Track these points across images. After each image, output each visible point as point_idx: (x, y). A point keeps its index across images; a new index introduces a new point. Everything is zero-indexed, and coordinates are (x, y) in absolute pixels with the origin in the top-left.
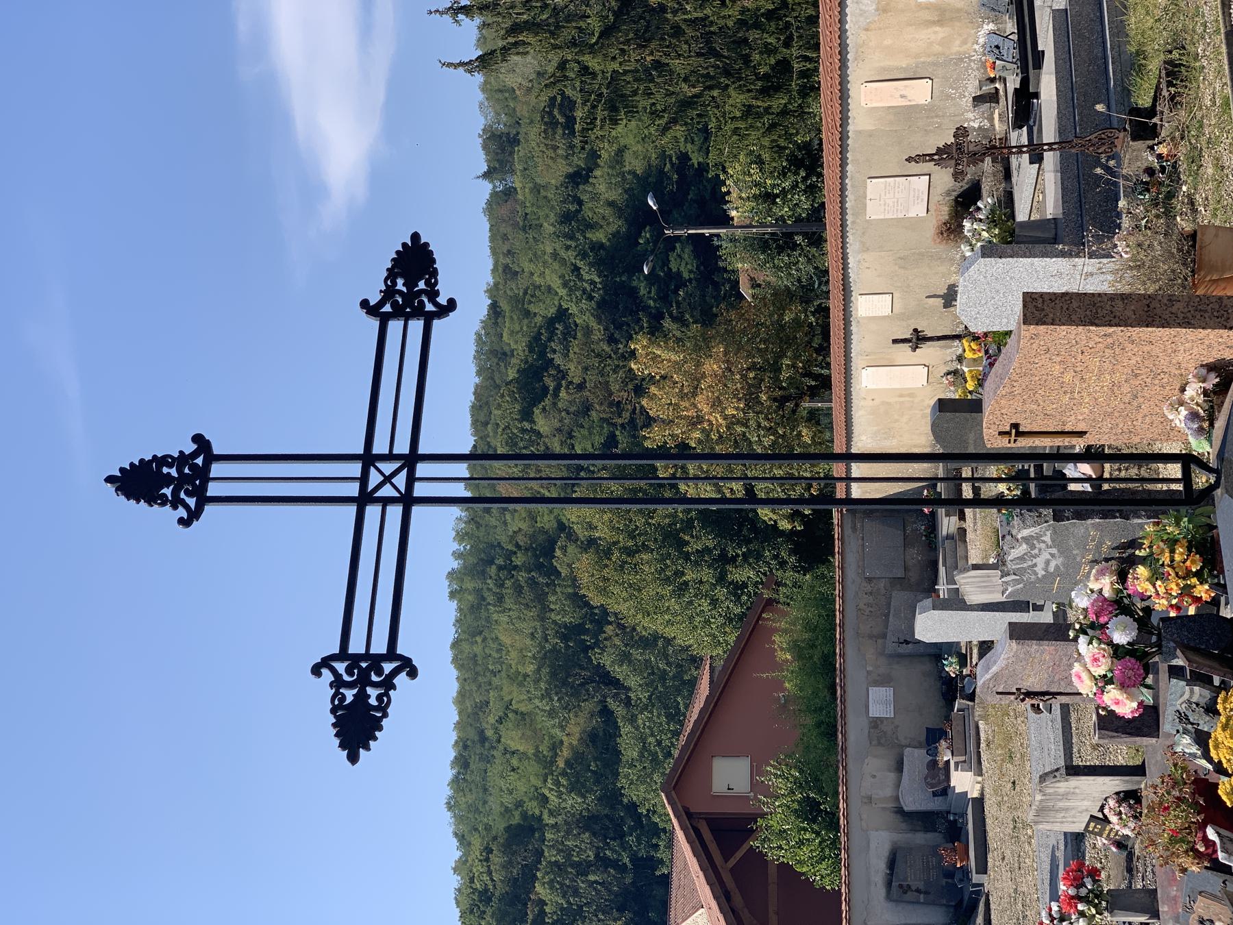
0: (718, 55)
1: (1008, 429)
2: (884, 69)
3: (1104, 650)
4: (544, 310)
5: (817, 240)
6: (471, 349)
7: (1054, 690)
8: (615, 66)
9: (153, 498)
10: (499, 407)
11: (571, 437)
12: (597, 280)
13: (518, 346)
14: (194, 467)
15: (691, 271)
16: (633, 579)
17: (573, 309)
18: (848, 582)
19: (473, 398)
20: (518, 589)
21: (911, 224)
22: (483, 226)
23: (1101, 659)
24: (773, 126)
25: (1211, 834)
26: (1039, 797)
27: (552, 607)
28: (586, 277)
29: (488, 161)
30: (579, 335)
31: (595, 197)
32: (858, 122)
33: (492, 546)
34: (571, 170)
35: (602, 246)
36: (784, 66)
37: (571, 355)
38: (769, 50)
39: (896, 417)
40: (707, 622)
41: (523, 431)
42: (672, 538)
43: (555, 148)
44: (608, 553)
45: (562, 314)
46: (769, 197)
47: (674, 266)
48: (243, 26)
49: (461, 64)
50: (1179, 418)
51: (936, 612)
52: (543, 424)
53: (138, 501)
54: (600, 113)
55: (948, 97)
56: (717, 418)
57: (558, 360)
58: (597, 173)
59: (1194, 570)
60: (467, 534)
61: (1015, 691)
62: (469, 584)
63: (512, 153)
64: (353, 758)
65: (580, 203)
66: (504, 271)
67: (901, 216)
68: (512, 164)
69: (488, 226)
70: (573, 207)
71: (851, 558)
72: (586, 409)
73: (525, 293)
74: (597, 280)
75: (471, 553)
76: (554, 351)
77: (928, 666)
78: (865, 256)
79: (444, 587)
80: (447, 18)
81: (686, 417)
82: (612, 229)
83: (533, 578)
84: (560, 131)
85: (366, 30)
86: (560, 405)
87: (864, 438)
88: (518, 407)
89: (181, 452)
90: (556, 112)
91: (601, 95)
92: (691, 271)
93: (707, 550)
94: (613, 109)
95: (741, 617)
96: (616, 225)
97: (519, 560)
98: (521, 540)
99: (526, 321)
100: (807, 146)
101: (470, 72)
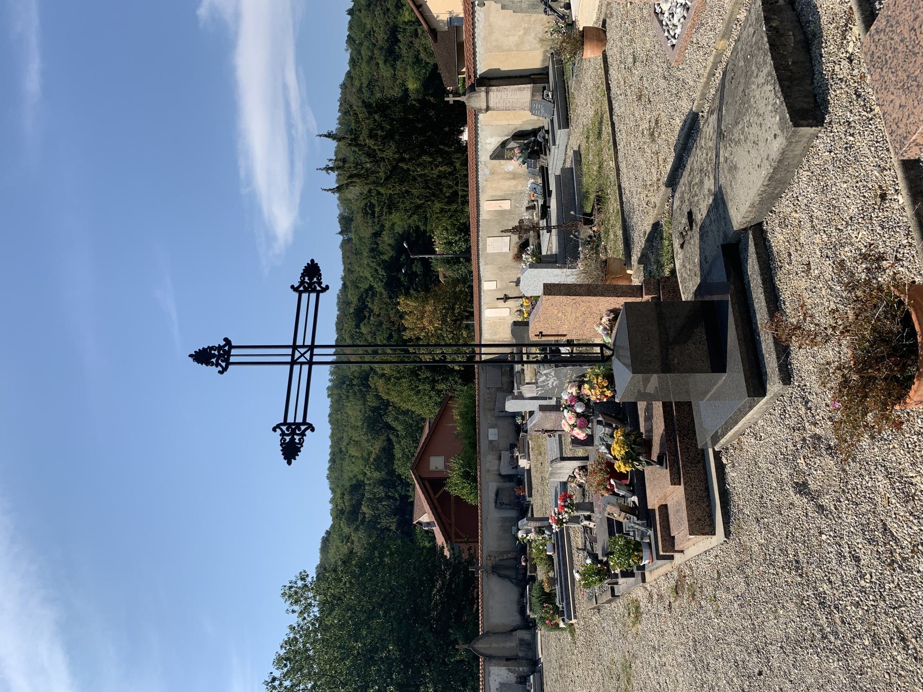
0: (430, 189)
2: (493, 196)
4: (364, 286)
5: (469, 260)
6: (336, 300)
8: (390, 192)
9: (208, 363)
13: (354, 300)
14: (224, 351)
15: (420, 271)
16: (399, 389)
17: (375, 286)
18: (481, 390)
20: (355, 393)
21: (503, 255)
22: (340, 253)
25: (612, 482)
28: (380, 273)
30: (378, 295)
31: (383, 242)
32: (484, 216)
34: (374, 232)
35: (386, 261)
36: (455, 193)
37: (375, 303)
38: (450, 187)
41: (356, 332)
42: (414, 373)
43: (367, 223)
44: (389, 379)
47: (414, 269)
48: (242, 173)
49: (330, 190)
50: (600, 330)
53: (202, 364)
54: (385, 210)
55: (517, 207)
57: (370, 305)
58: (384, 233)
60: (334, 372)
62: (335, 392)
63: (350, 225)
64: (289, 463)
65: (378, 244)
68: (351, 229)
69: (341, 253)
70: (375, 246)
72: (381, 324)
73: (357, 279)
75: (336, 380)
76: (368, 302)
79: (325, 393)
80: (324, 172)
82: (390, 255)
84: (369, 216)
86: (370, 322)
88: (354, 323)
93: (427, 378)
95: (440, 403)
96: (391, 253)
97: (355, 382)
101: (333, 193)
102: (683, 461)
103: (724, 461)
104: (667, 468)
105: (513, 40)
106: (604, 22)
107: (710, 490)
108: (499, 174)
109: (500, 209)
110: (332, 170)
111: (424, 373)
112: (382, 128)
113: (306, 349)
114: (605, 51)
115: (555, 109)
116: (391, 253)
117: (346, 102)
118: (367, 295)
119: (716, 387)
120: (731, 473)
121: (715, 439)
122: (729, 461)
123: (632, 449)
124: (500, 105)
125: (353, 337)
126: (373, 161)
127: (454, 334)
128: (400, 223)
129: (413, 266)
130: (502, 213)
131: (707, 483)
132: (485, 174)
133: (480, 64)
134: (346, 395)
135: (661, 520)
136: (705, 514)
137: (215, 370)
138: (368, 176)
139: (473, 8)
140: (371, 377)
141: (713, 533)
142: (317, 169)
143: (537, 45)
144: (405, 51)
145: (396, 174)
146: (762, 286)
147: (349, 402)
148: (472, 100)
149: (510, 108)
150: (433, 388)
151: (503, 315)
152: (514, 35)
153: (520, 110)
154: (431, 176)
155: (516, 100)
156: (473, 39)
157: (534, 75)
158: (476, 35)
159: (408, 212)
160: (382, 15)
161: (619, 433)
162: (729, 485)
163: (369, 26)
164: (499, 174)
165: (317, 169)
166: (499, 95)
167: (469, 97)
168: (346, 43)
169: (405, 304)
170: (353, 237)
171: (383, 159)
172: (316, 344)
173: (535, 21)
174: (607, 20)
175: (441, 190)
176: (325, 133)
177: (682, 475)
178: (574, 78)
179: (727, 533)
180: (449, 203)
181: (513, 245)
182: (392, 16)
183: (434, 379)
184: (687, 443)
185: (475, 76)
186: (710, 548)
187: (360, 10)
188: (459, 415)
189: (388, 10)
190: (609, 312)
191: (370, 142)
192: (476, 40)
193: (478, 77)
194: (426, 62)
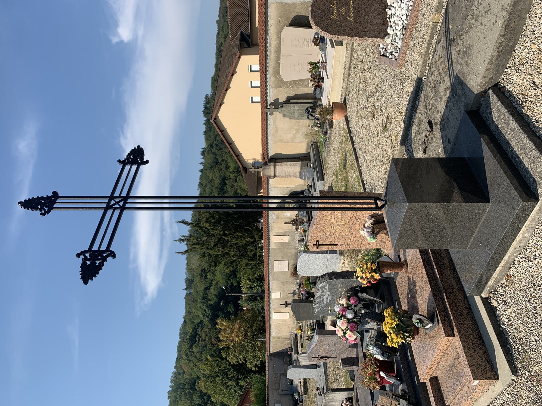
0: (240, 252)
1: (315, 243)
2: (278, 233)
3: (345, 320)
4: (197, 321)
5: (262, 299)
6: (179, 332)
7: (328, 356)
8: (216, 253)
10: (184, 345)
11: (202, 353)
12: (210, 313)
13: (190, 331)
15: (233, 311)
16: (215, 385)
17: (204, 320)
18: (269, 375)
19: (178, 344)
20: (186, 394)
21: (284, 273)
22: (184, 301)
23: (345, 323)
24: (252, 268)
25: (382, 374)
26: (324, 401)
27: (194, 399)
28: (208, 312)
29: (186, 286)
30: (205, 327)
31: (211, 293)
32: (272, 246)
33: (180, 384)
34: (206, 287)
35: (212, 305)
36: (255, 255)
37: (203, 332)
38: (251, 251)
39: (281, 327)
40: (233, 397)
41: (190, 351)
42: (225, 373)
43: (202, 282)
44: (208, 378)
45: (201, 322)
46: (251, 288)
47: (229, 310)
48: (132, 255)
49: (180, 253)
50: (365, 233)
51: (293, 369)
52: (195, 350)
53: (28, 209)
54: (213, 264)
55: (293, 240)
56: (237, 339)
57: (199, 333)
58: (212, 287)
59: (374, 268)
60: (174, 381)
61: (317, 356)
62: (173, 395)
63: (192, 284)
64: (86, 282)
65: (207, 294)
66: (188, 312)
67: (282, 271)
68: (192, 286)
69: (185, 301)
70: (206, 295)
71: (270, 368)
72: (206, 346)
73: (193, 317)
74: (210, 313)
75: (174, 386)
76: (199, 331)
77: (290, 397)
78: (274, 281)
79: (166, 396)
80: (178, 242)
81: (230, 339)
82: (215, 301)
83: (189, 391)
84: (203, 278)
85: (160, 257)
86: (199, 345)
87: (273, 333)
88: (189, 345)
89: (47, 196)
90: (203, 273)
91: (213, 260)
92: (233, 311)
93: (234, 377)
94: (215, 263)
95: (242, 395)
96: (215, 300)
97: (186, 387)
98: (187, 381)
99: (192, 324)
100: (260, 276)
101: (182, 254)
102: (453, 314)
103: (495, 304)
104: (439, 324)
105: (290, 136)
106: (345, 99)
107: (484, 338)
108: (282, 218)
109: (282, 241)
110: (183, 241)
111: (232, 373)
112: (214, 218)
114: (346, 115)
115: (315, 172)
116: (215, 300)
117: (195, 216)
118: (199, 327)
119: (474, 235)
120: (504, 313)
121: (480, 287)
122: (500, 302)
123: (401, 321)
124: (282, 174)
125: (188, 355)
126: (208, 236)
127: (252, 344)
128: (222, 281)
129: (228, 307)
130: (283, 244)
131: (479, 332)
132: (273, 219)
133: (271, 150)
134: (180, 396)
135: (434, 391)
136: (484, 359)
138: (204, 244)
139: (267, 116)
140: (197, 383)
141: (496, 377)
142: (174, 241)
143: (303, 140)
144: (229, 189)
145: (221, 242)
146: (511, 118)
147: (181, 401)
148: (266, 170)
149: (288, 176)
150: (237, 384)
151: (284, 318)
152: (290, 134)
153: (294, 177)
154: (241, 244)
155: (291, 171)
156: (267, 135)
157: (301, 157)
158: (268, 133)
159: (226, 265)
160: (218, 172)
161: (389, 310)
162: (504, 325)
163: (211, 177)
164: (282, 218)
165: (174, 241)
166: (281, 168)
167: (264, 169)
168: (198, 186)
169: (222, 323)
170: (193, 291)
171: (213, 235)
173: (302, 125)
174: (347, 97)
175: (246, 252)
176: (181, 220)
177: (454, 326)
178: (326, 149)
179: (514, 370)
180: (252, 260)
181: (290, 266)
182: (223, 172)
183: (238, 377)
184: (454, 299)
185: (267, 157)
186: (493, 398)
187: (206, 170)
188: (254, 397)
189: (221, 169)
190: (370, 217)
191: (206, 225)
192: (268, 136)
193: (269, 158)
194: (240, 194)
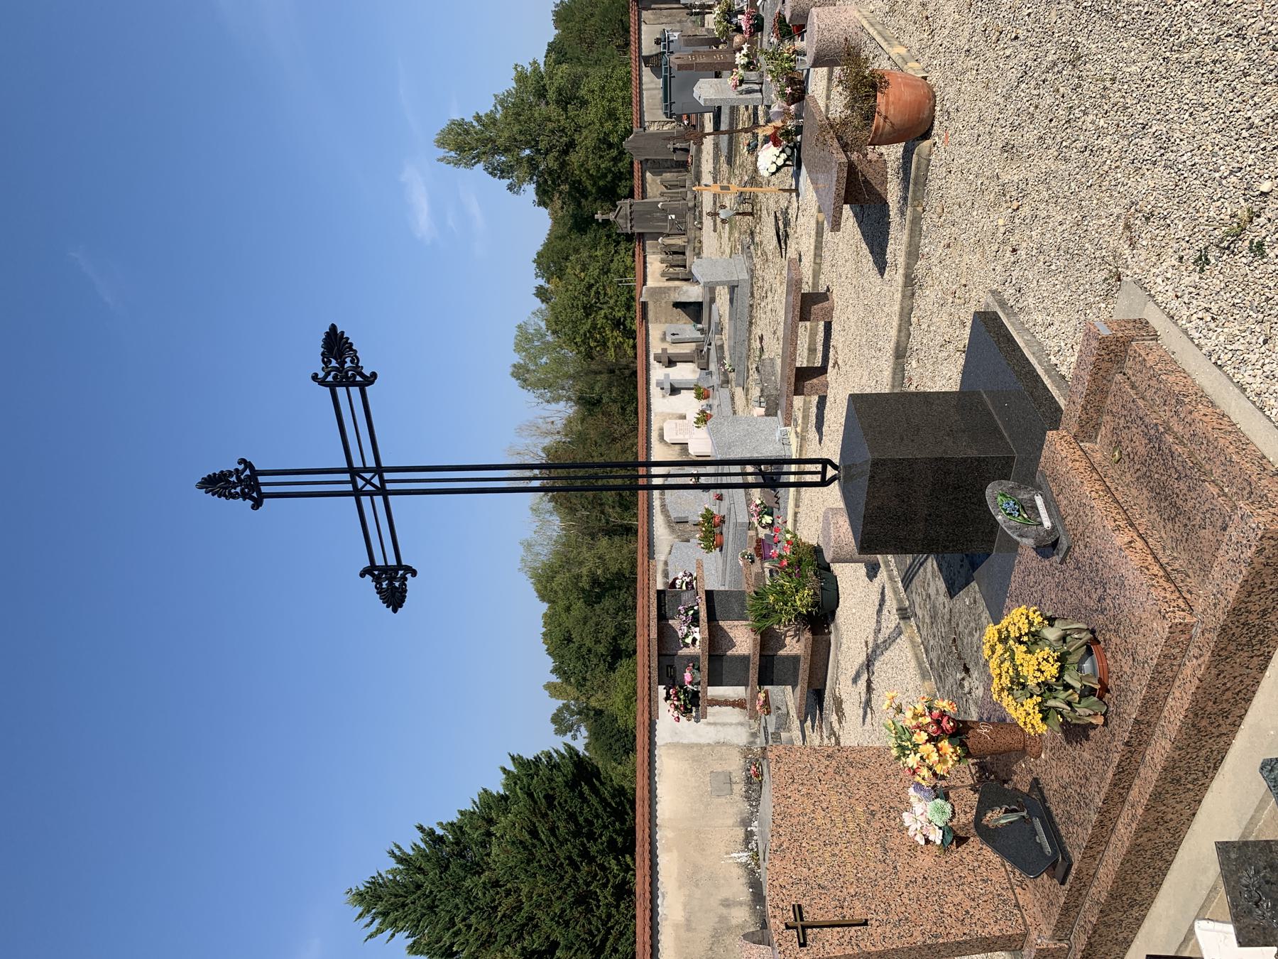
9: (326, 358)
14: (354, 376)
113: (358, 479)
137: (318, 368)
172: (390, 498)
